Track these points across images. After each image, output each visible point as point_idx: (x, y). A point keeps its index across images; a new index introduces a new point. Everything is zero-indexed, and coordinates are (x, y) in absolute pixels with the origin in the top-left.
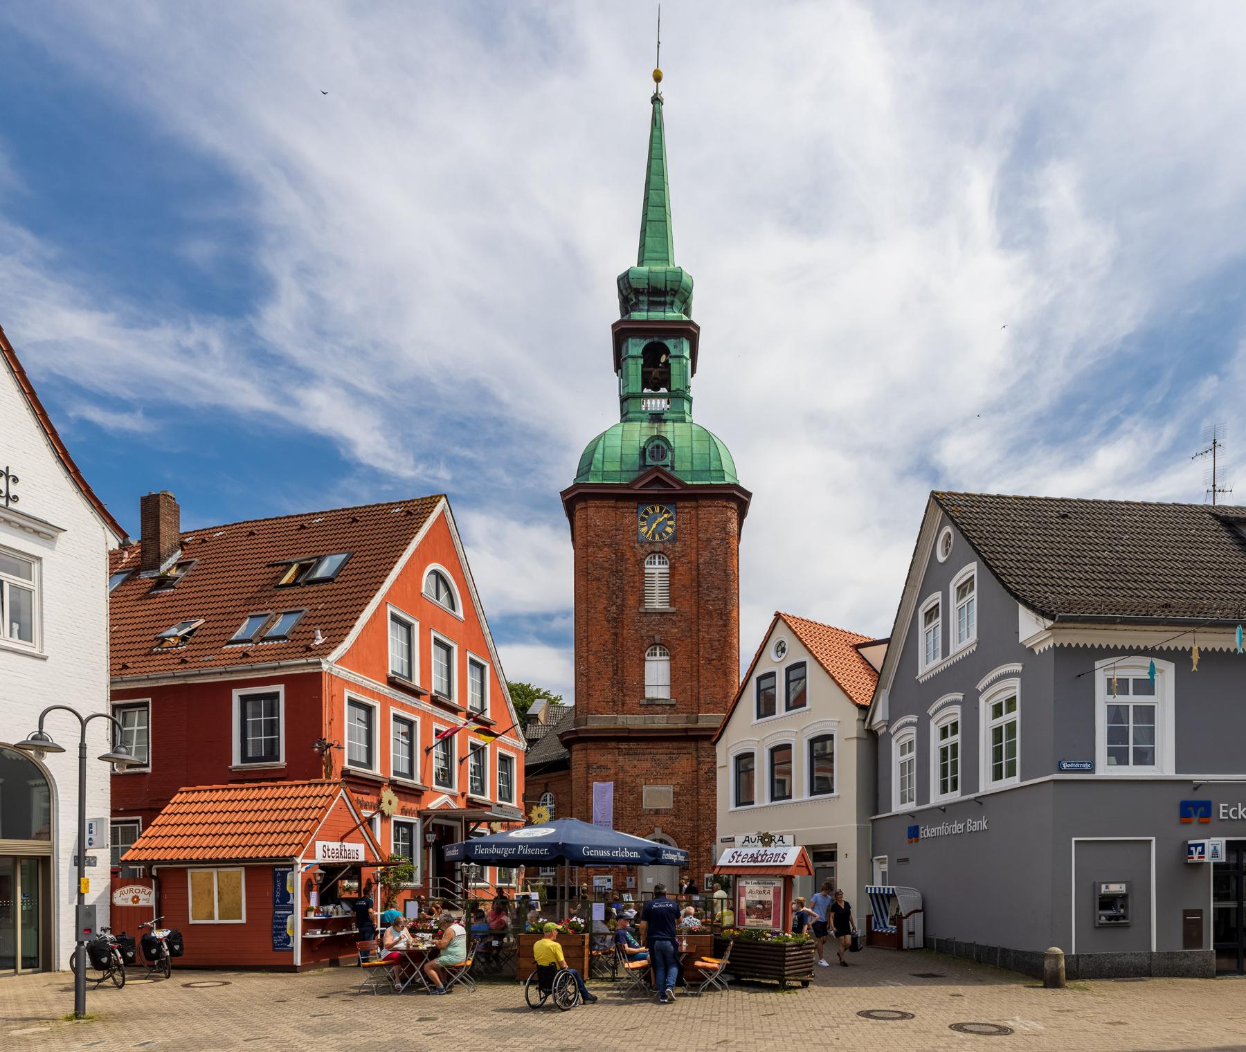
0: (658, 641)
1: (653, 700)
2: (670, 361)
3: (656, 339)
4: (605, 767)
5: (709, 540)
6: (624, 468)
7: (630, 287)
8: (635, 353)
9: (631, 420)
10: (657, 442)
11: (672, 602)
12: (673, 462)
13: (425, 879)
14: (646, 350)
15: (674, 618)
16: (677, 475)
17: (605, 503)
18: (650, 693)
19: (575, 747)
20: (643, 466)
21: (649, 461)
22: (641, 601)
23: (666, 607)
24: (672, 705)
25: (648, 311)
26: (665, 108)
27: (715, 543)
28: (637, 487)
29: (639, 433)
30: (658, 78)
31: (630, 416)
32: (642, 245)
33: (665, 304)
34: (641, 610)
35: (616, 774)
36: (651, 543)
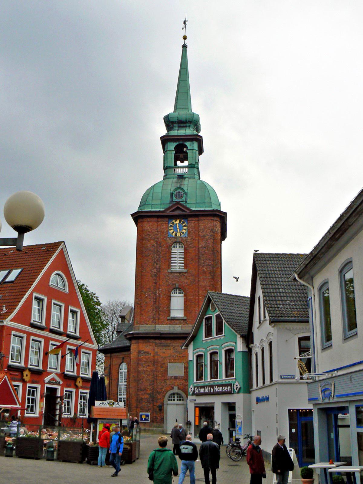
0: (177, 286)
1: (174, 317)
2: (188, 151)
3: (181, 142)
4: (148, 353)
5: (204, 236)
6: (162, 203)
7: (169, 121)
8: (171, 149)
9: (168, 178)
10: (179, 190)
11: (186, 266)
12: (186, 199)
13: (40, 414)
14: (176, 148)
15: (186, 275)
16: (188, 206)
17: (152, 219)
18: (174, 314)
19: (133, 341)
20: (171, 201)
21: (175, 199)
22: (169, 266)
23: (182, 269)
24: (184, 320)
25: (178, 130)
26: (188, 50)
27: (207, 237)
28: (168, 212)
29: (171, 186)
30: (185, 38)
31: (168, 176)
32: (176, 103)
33: (186, 127)
34: (169, 271)
35: (154, 356)
36: (174, 238)
